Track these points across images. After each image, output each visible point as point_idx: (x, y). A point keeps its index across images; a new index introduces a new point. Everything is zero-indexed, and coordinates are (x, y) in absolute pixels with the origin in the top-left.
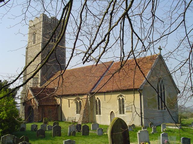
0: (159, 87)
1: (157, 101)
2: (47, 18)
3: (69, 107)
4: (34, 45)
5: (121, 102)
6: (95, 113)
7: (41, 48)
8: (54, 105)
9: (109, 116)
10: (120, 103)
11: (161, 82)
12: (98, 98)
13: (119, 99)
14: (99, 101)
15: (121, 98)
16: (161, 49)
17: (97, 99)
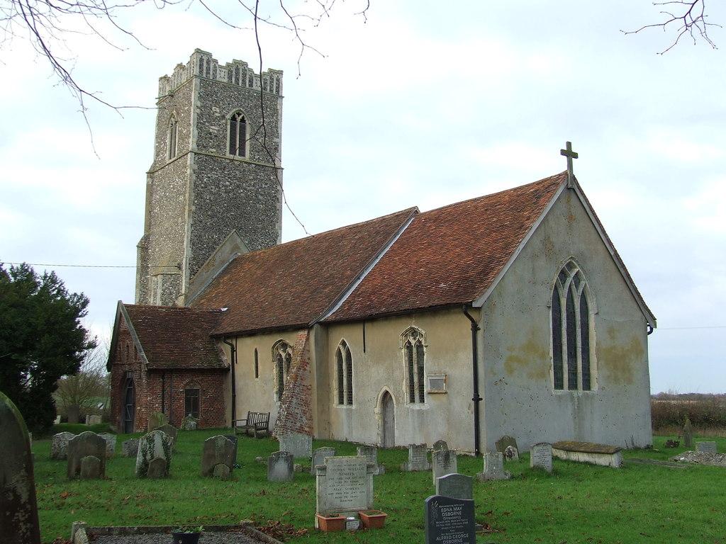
0: (564, 302)
3: (257, 377)
4: (173, 159)
5: (415, 355)
6: (336, 399)
8: (208, 369)
9: (378, 410)
12: (344, 343)
13: (409, 347)
16: (576, 156)
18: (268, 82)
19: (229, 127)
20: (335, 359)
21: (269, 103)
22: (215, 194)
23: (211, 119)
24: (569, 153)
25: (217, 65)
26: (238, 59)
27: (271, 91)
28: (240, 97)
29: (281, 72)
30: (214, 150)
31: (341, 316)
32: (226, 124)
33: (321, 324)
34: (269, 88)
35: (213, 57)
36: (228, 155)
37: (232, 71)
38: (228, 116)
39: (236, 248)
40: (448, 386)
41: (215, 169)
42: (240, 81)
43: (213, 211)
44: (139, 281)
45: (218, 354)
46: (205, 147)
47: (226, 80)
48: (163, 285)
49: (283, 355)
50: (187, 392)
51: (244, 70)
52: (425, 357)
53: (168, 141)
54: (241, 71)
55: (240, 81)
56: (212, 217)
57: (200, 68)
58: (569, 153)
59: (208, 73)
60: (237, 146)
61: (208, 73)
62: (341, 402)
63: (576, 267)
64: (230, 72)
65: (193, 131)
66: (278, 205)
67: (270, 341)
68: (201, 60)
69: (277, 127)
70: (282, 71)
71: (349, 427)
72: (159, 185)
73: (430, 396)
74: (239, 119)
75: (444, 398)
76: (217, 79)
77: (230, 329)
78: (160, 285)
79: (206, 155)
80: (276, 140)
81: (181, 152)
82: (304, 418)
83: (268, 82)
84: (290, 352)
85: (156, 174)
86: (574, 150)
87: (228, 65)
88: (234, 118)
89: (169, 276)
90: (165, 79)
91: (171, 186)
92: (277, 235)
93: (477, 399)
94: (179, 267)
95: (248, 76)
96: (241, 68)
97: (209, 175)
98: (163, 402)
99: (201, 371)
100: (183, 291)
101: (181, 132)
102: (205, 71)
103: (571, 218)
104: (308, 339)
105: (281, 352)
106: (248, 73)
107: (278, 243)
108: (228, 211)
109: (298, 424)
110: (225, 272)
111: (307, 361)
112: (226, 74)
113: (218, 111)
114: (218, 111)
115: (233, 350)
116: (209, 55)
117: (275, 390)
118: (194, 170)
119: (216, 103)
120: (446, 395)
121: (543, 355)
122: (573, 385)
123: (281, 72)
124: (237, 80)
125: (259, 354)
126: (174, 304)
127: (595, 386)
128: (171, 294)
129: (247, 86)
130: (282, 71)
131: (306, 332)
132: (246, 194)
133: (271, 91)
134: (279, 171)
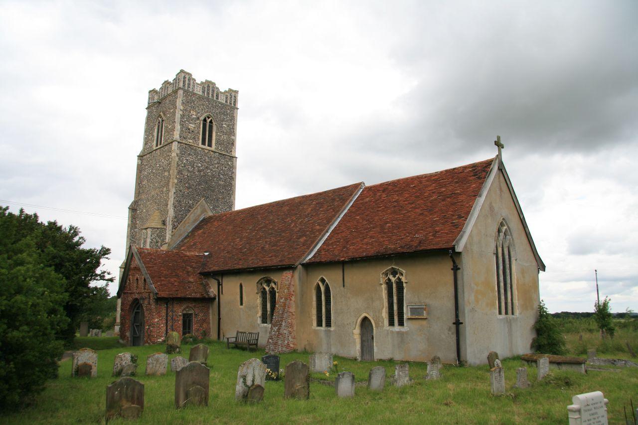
2: (192, 82)
3: (242, 304)
4: (159, 147)
5: (396, 292)
9: (357, 331)
11: (502, 234)
12: (323, 280)
13: (389, 284)
17: (321, 284)
18: (229, 98)
19: (202, 125)
23: (190, 119)
26: (209, 79)
27: (231, 104)
29: (236, 92)
30: (191, 141)
31: (318, 260)
32: (200, 124)
33: (303, 265)
35: (193, 77)
36: (201, 145)
37: (205, 88)
38: (202, 118)
39: (204, 211)
40: (428, 314)
41: (192, 154)
42: (210, 95)
43: (189, 184)
44: (129, 233)
45: (206, 286)
46: (185, 138)
47: (201, 93)
48: (151, 236)
49: (267, 289)
50: (184, 315)
51: (213, 87)
52: (405, 291)
53: (155, 134)
54: (211, 87)
55: (210, 95)
56: (188, 188)
60: (207, 138)
62: (319, 324)
63: (505, 226)
64: (204, 88)
65: (178, 127)
66: (233, 182)
67: (257, 278)
68: (185, 78)
70: (238, 91)
71: (328, 344)
72: (147, 165)
73: (410, 322)
74: (208, 121)
75: (424, 323)
76: (195, 92)
78: (149, 235)
79: (186, 144)
80: (233, 137)
81: (166, 141)
82: (290, 338)
83: (229, 98)
84: (274, 286)
85: (145, 157)
86: (502, 142)
87: (202, 83)
88: (205, 120)
89: (156, 229)
90: (153, 92)
91: (158, 165)
92: (231, 204)
94: (164, 223)
95: (215, 92)
97: (187, 158)
98: (167, 323)
99: (195, 300)
100: (167, 240)
101: (166, 127)
103: (501, 190)
105: (265, 287)
107: (233, 210)
108: (200, 184)
109: (286, 342)
110: (197, 228)
111: (292, 293)
112: (201, 89)
119: (193, 108)
120: (427, 320)
121: (493, 289)
122: (506, 313)
123: (236, 92)
124: (208, 93)
125: (244, 288)
128: (157, 242)
130: (238, 91)
132: (212, 173)
133: (231, 104)
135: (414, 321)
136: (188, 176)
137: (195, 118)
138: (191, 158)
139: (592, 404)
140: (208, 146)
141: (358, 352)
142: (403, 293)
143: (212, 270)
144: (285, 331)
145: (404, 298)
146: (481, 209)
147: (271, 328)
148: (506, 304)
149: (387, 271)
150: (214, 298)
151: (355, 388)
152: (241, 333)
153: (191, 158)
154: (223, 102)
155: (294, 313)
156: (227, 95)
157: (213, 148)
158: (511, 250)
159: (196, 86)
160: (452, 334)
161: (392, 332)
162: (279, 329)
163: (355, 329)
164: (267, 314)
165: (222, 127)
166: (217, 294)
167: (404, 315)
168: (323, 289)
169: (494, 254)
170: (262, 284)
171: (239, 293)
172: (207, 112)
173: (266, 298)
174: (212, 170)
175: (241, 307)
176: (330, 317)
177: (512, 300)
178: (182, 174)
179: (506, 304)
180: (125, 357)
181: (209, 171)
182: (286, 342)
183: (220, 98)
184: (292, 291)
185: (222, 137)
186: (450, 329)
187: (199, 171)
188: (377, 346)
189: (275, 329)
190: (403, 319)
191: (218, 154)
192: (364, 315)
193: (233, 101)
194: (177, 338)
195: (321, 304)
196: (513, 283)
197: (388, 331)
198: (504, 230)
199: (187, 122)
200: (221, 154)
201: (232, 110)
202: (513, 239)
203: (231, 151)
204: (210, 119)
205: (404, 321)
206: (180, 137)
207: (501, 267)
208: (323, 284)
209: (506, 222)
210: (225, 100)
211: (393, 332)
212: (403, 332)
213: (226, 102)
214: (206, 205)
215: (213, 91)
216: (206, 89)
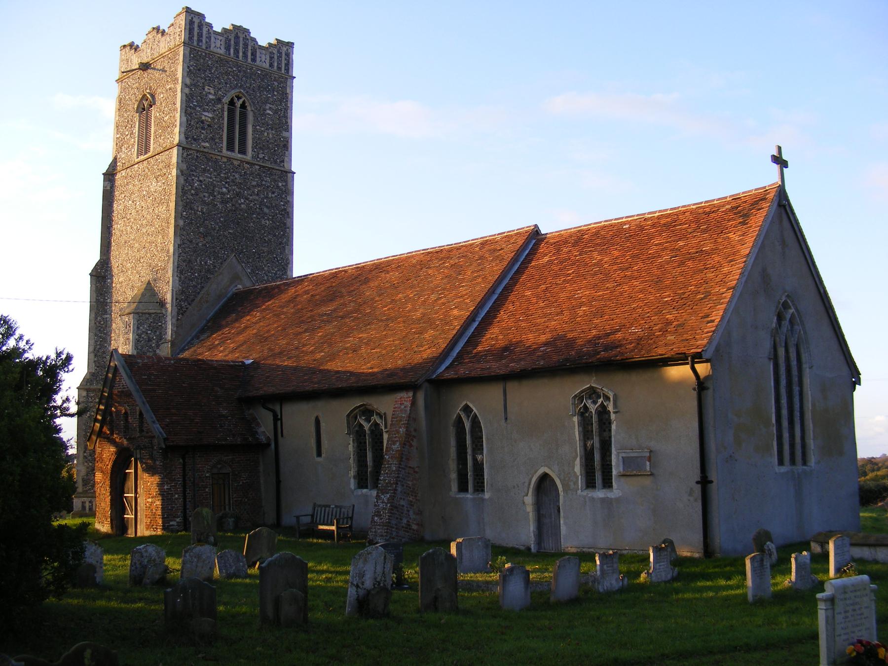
1: (774, 421)
2: (205, 30)
3: (319, 454)
7: (174, 172)
9: (529, 499)
10: (586, 434)
11: (786, 324)
12: (467, 409)
14: (475, 423)
15: (593, 408)
17: (463, 416)
18: (276, 57)
19: (226, 114)
20: (452, 431)
21: (276, 84)
22: (208, 204)
24: (779, 161)
25: (211, 31)
28: (240, 74)
29: (290, 45)
30: (207, 144)
32: (223, 111)
33: (430, 381)
34: (276, 64)
35: (207, 20)
38: (226, 100)
39: (236, 278)
41: (209, 170)
42: (241, 54)
44: (93, 322)
46: (195, 140)
47: (222, 51)
48: (138, 328)
49: (367, 426)
51: (245, 39)
52: (614, 427)
54: (241, 39)
55: (241, 54)
57: (190, 34)
58: (779, 161)
59: (199, 41)
60: (236, 141)
61: (199, 41)
62: (463, 488)
69: (286, 117)
70: (293, 44)
73: (623, 479)
74: (239, 103)
77: (271, 390)
79: (198, 151)
80: (285, 134)
82: (411, 512)
83: (276, 57)
88: (232, 103)
89: (147, 316)
92: (286, 262)
93: (705, 482)
95: (250, 48)
96: (241, 36)
97: (201, 178)
98: (184, 492)
102: (195, 38)
103: (783, 243)
104: (414, 403)
105: (362, 422)
106: (250, 44)
109: (405, 521)
111: (413, 433)
113: (212, 91)
114: (212, 91)
115: (277, 419)
116: (201, 16)
117: (352, 473)
118: (182, 171)
119: (210, 82)
122: (793, 462)
123: (290, 45)
124: (237, 51)
126: (155, 354)
127: (812, 460)
128: (150, 340)
129: (249, 60)
130: (293, 44)
131: (411, 394)
132: (248, 205)
133: (279, 68)
134: (289, 175)
135: (629, 479)
136: (203, 213)
137: (213, 100)
138: (207, 177)
139: (851, 592)
140: (239, 152)
141: (532, 534)
142: (610, 430)
143: (261, 392)
144: (402, 501)
145: (613, 439)
146: (746, 282)
147: (378, 497)
148: (792, 446)
149: (582, 392)
150: (269, 445)
151: (531, 593)
152: (320, 506)
153: (207, 177)
154: (264, 65)
155: (416, 470)
156: (272, 53)
157: (249, 156)
158: (802, 351)
159: (213, 39)
160: (696, 500)
161: (593, 499)
162: (392, 498)
163: (527, 495)
164: (366, 472)
165: (264, 115)
166: (272, 437)
167: (614, 470)
168: (467, 425)
169: (770, 359)
170: (356, 418)
171: (314, 434)
172: (236, 87)
173: (365, 443)
174: (247, 199)
175: (319, 459)
176: (483, 475)
177: (803, 438)
178: (191, 209)
179: (792, 446)
180: (146, 551)
181: (242, 201)
182: (405, 521)
183: (258, 59)
184: (412, 429)
185: (266, 134)
186: (691, 493)
187: (224, 202)
188: (565, 523)
189: (385, 497)
190: (611, 476)
191: (258, 167)
192: (541, 471)
193: (284, 62)
194: (210, 518)
195: (466, 453)
196: (805, 408)
197: (585, 497)
198: (788, 317)
199: (198, 109)
200: (264, 167)
201: (281, 82)
202: (805, 332)
203: (283, 161)
204: (241, 101)
205: (613, 479)
206: (187, 138)
207: (783, 382)
208: (468, 417)
209: (792, 301)
210: (268, 61)
211: (593, 498)
212: (611, 499)
213: (271, 65)
214: (239, 267)
215: (246, 46)
216: (232, 42)
